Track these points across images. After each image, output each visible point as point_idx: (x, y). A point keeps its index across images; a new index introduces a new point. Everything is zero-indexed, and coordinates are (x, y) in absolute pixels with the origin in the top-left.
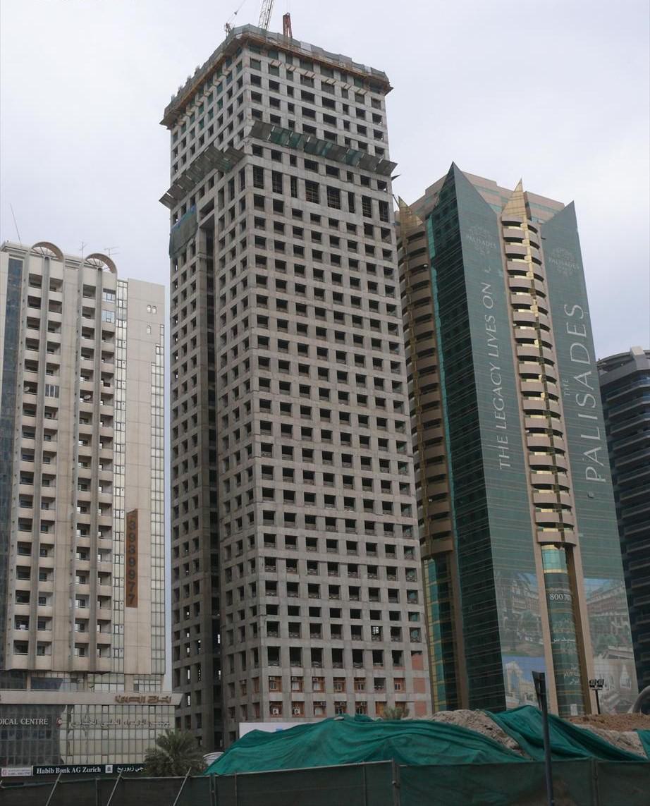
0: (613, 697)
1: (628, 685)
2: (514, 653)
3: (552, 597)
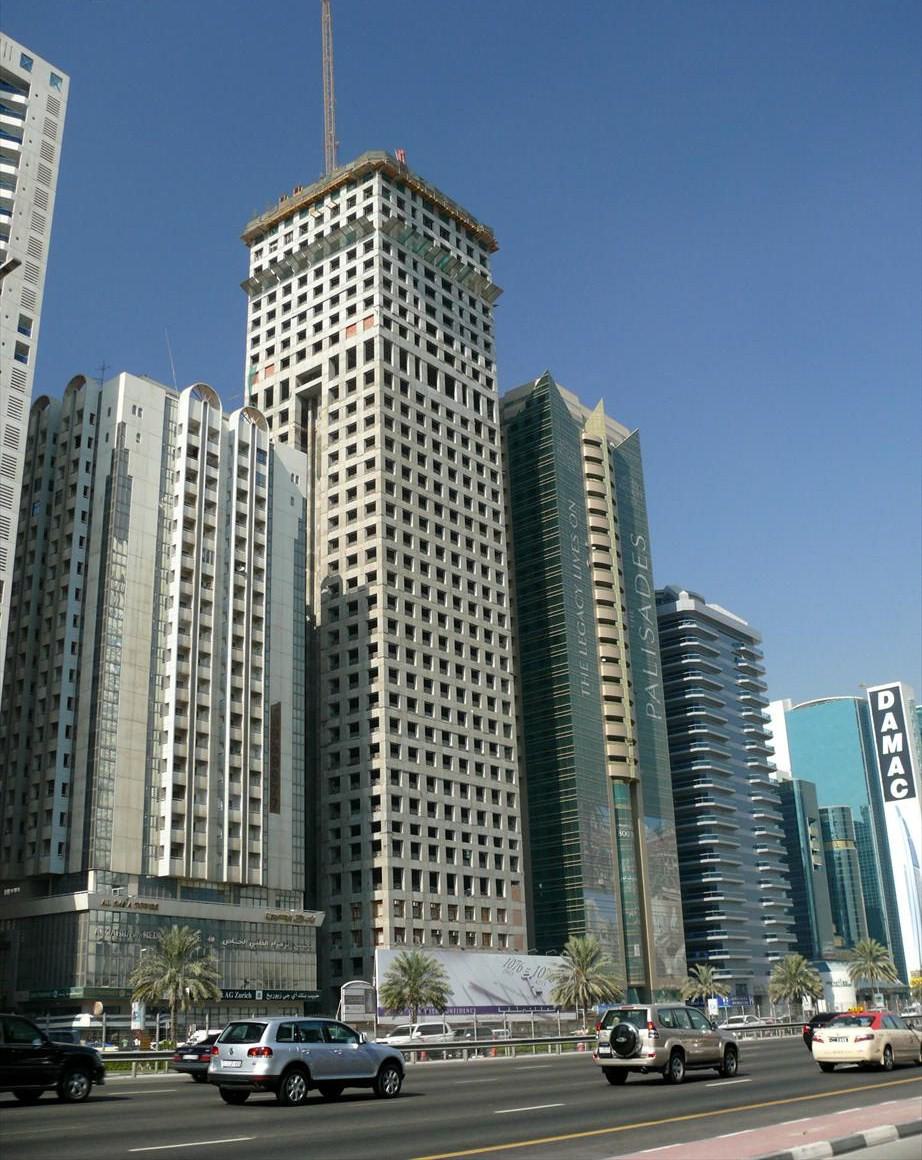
0: (665, 939)
1: (676, 928)
2: (592, 889)
3: (621, 833)
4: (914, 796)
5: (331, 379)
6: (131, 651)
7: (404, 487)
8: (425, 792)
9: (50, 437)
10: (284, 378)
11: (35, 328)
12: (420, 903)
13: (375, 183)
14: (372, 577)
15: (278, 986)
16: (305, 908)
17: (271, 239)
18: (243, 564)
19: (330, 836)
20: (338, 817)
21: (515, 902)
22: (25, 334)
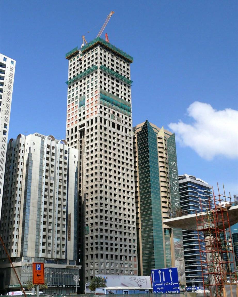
6: (33, 203)
8: (110, 234)
9: (13, 149)
10: (76, 126)
11: (8, 127)
15: (69, 284)
22: (6, 128)
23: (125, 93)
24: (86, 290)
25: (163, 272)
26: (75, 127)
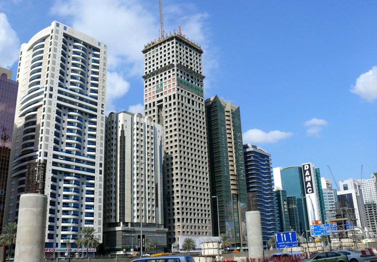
3: (234, 207)
4: (313, 192)
5: (165, 103)
7: (183, 129)
10: (154, 101)
12: (188, 226)
13: (174, 41)
14: (176, 151)
16: (164, 228)
17: (149, 52)
18: (149, 153)
19: (168, 210)
20: (170, 206)
21: (209, 225)
23: (181, 61)
24: (172, 249)
25: (285, 235)
26: (153, 102)
